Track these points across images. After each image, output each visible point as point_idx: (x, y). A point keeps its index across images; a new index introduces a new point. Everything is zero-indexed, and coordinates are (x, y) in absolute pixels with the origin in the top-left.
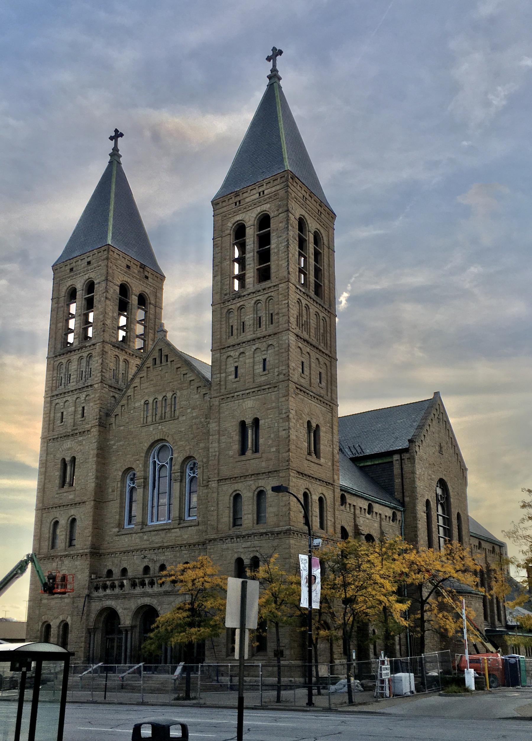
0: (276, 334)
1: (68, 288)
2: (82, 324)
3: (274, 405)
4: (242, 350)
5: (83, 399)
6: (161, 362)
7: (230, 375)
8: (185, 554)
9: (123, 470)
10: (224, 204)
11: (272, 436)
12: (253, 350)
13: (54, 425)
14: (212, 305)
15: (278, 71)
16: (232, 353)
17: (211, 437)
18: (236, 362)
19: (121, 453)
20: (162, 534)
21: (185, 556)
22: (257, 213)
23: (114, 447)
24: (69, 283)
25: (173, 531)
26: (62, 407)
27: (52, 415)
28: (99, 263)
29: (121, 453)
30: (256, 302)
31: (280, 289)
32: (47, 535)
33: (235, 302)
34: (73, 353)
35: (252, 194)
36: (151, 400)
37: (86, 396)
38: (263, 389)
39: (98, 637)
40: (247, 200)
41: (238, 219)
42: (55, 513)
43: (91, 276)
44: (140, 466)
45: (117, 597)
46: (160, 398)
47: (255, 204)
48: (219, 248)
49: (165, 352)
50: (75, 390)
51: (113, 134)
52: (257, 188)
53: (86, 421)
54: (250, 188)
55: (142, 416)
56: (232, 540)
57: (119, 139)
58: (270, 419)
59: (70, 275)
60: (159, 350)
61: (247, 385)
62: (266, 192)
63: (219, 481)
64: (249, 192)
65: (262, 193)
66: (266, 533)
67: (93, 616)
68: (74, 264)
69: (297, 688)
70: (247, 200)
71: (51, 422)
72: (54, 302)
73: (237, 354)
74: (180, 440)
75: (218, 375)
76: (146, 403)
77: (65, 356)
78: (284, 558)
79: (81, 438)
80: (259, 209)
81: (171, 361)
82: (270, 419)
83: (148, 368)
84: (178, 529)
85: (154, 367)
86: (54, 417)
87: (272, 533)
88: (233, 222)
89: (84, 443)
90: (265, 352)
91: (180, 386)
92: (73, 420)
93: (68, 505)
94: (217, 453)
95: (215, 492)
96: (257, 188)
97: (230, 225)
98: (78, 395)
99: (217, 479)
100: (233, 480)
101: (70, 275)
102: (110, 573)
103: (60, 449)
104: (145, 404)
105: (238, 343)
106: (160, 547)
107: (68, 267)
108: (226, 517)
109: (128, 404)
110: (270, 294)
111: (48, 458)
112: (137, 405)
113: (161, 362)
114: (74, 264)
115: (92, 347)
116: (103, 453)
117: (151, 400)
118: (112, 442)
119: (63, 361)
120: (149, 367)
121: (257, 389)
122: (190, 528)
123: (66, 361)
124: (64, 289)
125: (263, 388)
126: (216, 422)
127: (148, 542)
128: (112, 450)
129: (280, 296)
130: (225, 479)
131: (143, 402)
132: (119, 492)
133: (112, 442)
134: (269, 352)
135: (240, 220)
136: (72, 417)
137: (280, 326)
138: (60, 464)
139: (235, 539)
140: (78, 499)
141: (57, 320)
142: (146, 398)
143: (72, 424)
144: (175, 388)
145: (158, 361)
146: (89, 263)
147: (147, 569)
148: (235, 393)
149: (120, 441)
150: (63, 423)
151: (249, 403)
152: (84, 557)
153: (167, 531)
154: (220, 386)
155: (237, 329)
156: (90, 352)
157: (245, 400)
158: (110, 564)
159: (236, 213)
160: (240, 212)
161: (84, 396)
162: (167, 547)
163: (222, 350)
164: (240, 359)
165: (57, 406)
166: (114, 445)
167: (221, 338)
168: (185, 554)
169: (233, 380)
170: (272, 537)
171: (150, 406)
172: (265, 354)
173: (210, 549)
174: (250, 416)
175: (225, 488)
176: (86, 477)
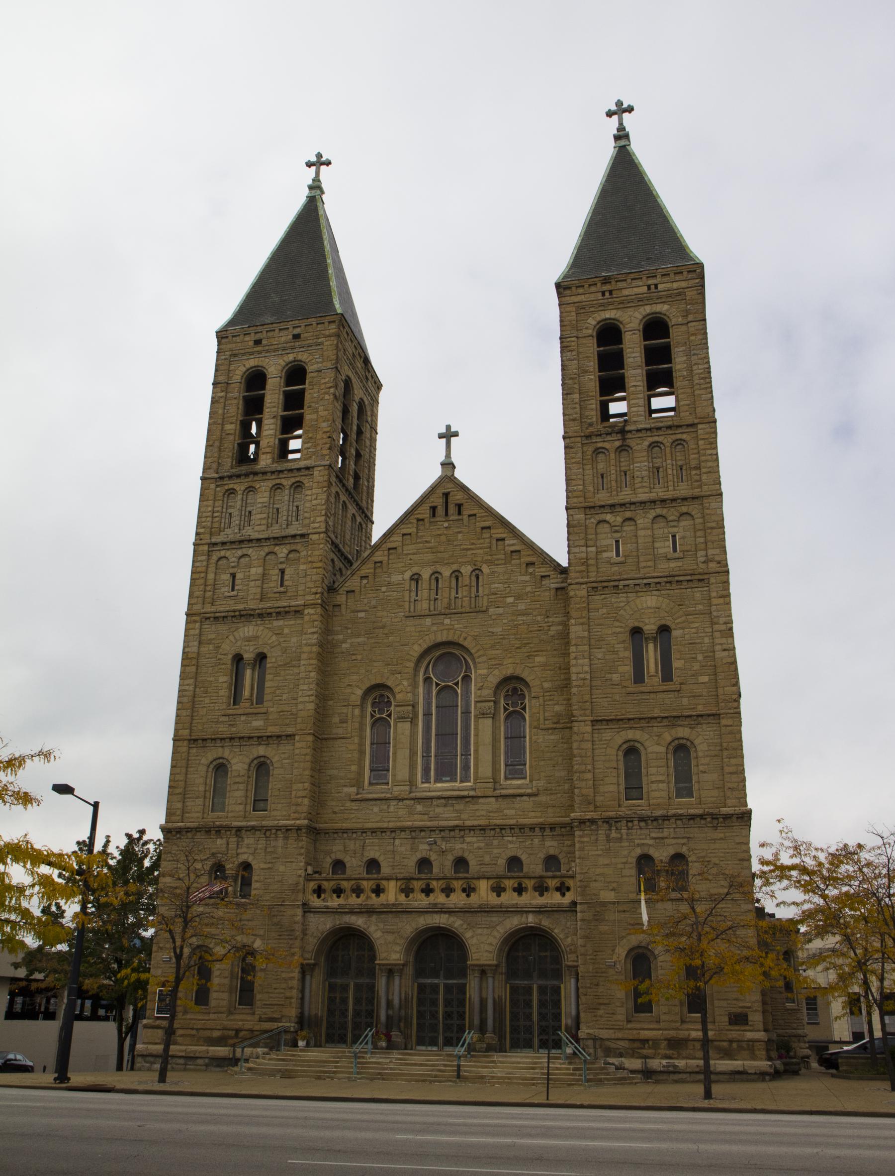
0: (697, 498)
1: (248, 370)
2: (278, 433)
3: (700, 607)
4: (628, 514)
5: (284, 555)
6: (447, 514)
7: (605, 551)
8: (511, 842)
9: (364, 688)
10: (581, 291)
11: (700, 657)
12: (651, 517)
13: (214, 595)
14: (564, 438)
15: (323, 192)
16: (608, 517)
17: (573, 649)
18: (616, 531)
19: (359, 657)
20: (459, 806)
21: (510, 846)
22: (644, 313)
23: (344, 645)
24: (252, 363)
25: (481, 800)
26: (232, 564)
27: (211, 576)
28: (320, 340)
29: (359, 657)
30: (650, 445)
31: (700, 432)
32: (202, 788)
33: (609, 438)
34: (260, 477)
35: (634, 285)
36: (426, 574)
37: (290, 552)
38: (677, 581)
39: (317, 983)
40: (626, 292)
41: (608, 316)
42: (220, 749)
43: (300, 358)
44: (405, 683)
45: (370, 911)
46: (446, 572)
47: (640, 301)
48: (574, 353)
49: (458, 497)
50: (266, 539)
51: (314, 159)
52: (644, 278)
53: (289, 594)
54: (632, 276)
55: (407, 599)
56: (630, 824)
57: (323, 168)
58: (694, 630)
59: (255, 349)
60: (443, 494)
61: (642, 571)
62: (660, 287)
63: (594, 722)
64: (629, 281)
65: (653, 287)
66: (702, 817)
67: (312, 942)
68: (264, 335)
69: (705, 1087)
70: (626, 292)
71: (208, 588)
72: (218, 389)
73: (619, 519)
74: (493, 647)
75: (583, 549)
76: (416, 578)
77: (242, 479)
78: (740, 860)
79: (281, 623)
80: (648, 309)
81: (470, 516)
82: (694, 630)
83: (418, 520)
84: (493, 800)
85: (432, 520)
86: (215, 580)
87: (714, 817)
88: (599, 319)
89: (286, 631)
90: (675, 523)
91: (489, 558)
92: (259, 590)
93: (252, 738)
94: (588, 677)
95: (587, 741)
96: (644, 278)
97: (592, 322)
98: (271, 548)
99: (592, 719)
100: (625, 723)
101: (255, 349)
102: (339, 865)
103: (231, 637)
104: (411, 579)
105: (622, 502)
106: (457, 826)
107: (253, 337)
108: (613, 785)
109: (375, 575)
110: (679, 436)
111: (202, 649)
112: (396, 578)
113: (447, 514)
114: (264, 335)
115: (304, 472)
116: (326, 654)
117: (426, 574)
118: (341, 637)
119: (284, 482)
120: (423, 520)
121: (665, 579)
122: (518, 798)
123: (243, 488)
124: (239, 372)
125: (677, 578)
126: (582, 624)
127: (426, 816)
128: (339, 650)
129: (701, 442)
130: (607, 720)
131: (407, 575)
132: (357, 725)
133: (341, 637)
134: (682, 523)
135: (610, 319)
136: (259, 583)
137: (705, 488)
138: (229, 662)
139: (636, 823)
140: (272, 730)
141: (223, 418)
142: (415, 570)
143: (258, 596)
144: (479, 559)
145: (440, 511)
146: (258, 342)
147: (424, 864)
148: (619, 580)
149: (359, 636)
150: (235, 593)
151: (650, 600)
152: (293, 834)
153: (468, 800)
154: (587, 566)
155: (616, 481)
156: (297, 479)
157: (640, 594)
158: (337, 849)
159: (604, 307)
160: (611, 307)
161: (285, 551)
162: (472, 828)
163: (588, 510)
164: (625, 528)
165: (220, 562)
166: (344, 642)
167: (584, 491)
168: (511, 842)
169: (226, 594)
170: (711, 823)
171: (424, 584)
172: (674, 526)
173: (581, 837)
174: (652, 621)
175: (607, 735)
176: (292, 691)
